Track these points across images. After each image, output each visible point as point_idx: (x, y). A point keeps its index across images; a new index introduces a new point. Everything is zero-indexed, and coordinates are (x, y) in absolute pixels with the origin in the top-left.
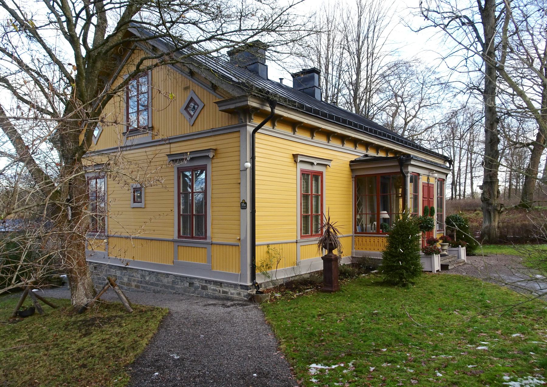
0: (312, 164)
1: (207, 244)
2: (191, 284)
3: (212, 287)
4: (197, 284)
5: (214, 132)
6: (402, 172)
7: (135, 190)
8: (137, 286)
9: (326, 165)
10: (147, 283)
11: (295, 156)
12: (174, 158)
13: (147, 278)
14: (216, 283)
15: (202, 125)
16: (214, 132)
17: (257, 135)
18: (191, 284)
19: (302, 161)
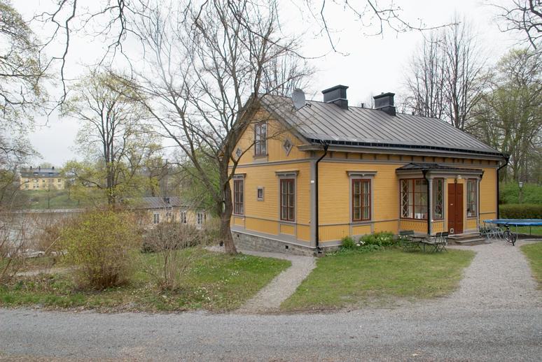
0: (283, 175)
1: (372, 222)
2: (287, 247)
3: (297, 249)
4: (290, 247)
5: (298, 161)
6: (425, 178)
7: (259, 190)
8: (260, 247)
9: (374, 175)
10: (265, 246)
11: (347, 172)
12: (279, 174)
13: (265, 243)
14: (298, 246)
15: (292, 157)
16: (298, 161)
17: (319, 163)
18: (287, 247)
19: (352, 175)
